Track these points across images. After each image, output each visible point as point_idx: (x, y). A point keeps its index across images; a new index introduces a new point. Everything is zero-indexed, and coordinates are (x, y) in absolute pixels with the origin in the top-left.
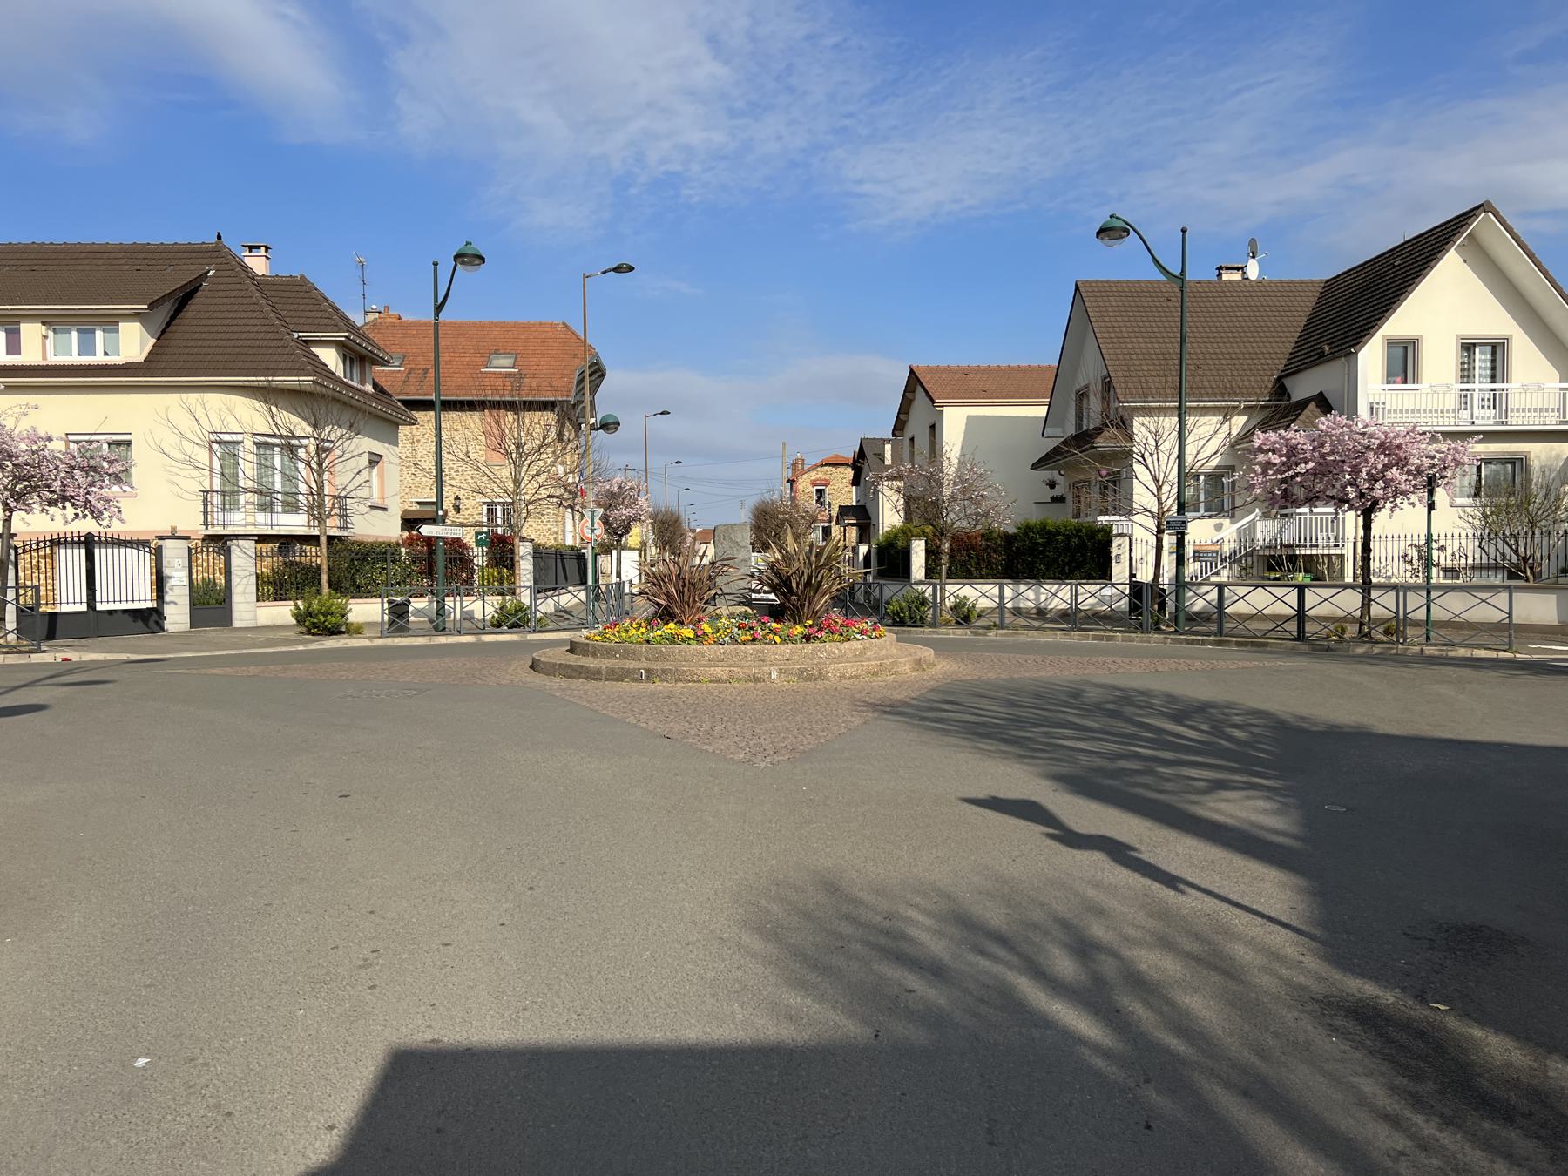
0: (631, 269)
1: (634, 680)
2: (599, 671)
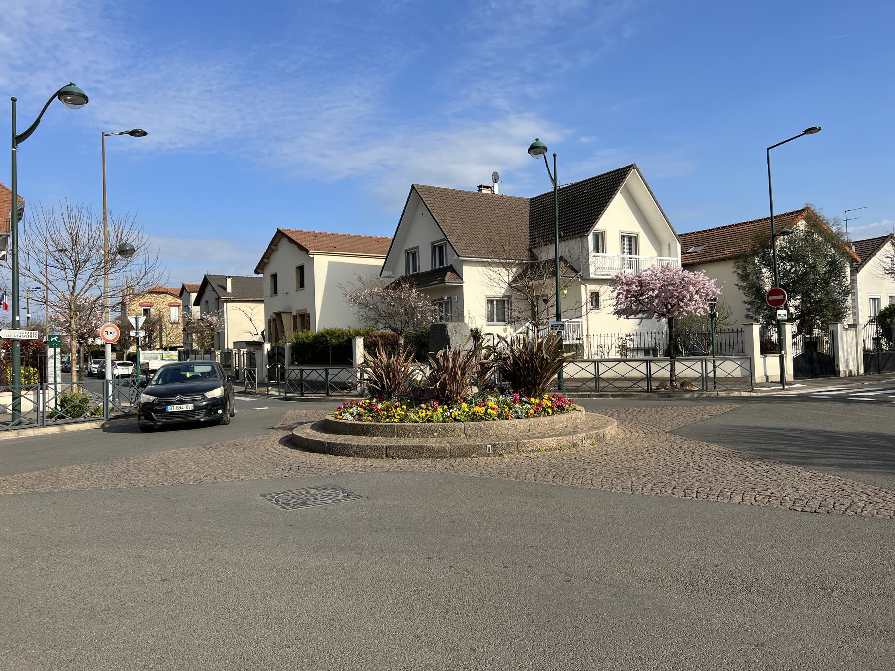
0: (144, 134)
1: (483, 455)
2: (443, 450)
